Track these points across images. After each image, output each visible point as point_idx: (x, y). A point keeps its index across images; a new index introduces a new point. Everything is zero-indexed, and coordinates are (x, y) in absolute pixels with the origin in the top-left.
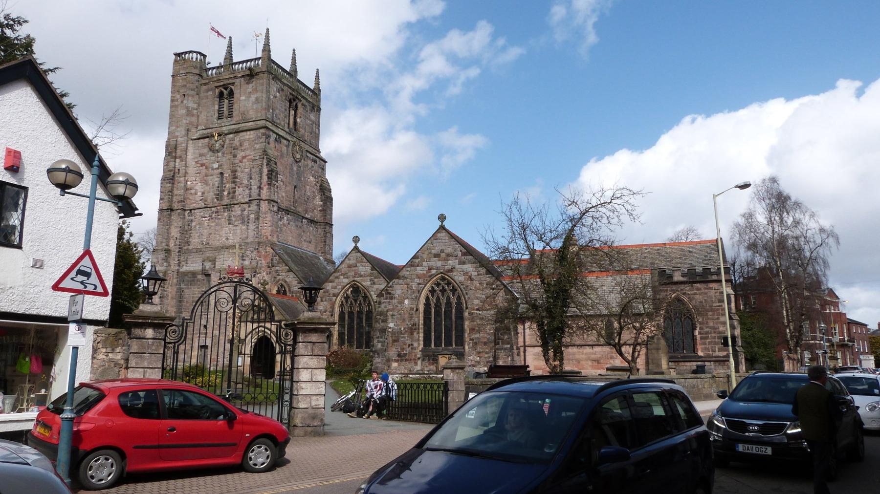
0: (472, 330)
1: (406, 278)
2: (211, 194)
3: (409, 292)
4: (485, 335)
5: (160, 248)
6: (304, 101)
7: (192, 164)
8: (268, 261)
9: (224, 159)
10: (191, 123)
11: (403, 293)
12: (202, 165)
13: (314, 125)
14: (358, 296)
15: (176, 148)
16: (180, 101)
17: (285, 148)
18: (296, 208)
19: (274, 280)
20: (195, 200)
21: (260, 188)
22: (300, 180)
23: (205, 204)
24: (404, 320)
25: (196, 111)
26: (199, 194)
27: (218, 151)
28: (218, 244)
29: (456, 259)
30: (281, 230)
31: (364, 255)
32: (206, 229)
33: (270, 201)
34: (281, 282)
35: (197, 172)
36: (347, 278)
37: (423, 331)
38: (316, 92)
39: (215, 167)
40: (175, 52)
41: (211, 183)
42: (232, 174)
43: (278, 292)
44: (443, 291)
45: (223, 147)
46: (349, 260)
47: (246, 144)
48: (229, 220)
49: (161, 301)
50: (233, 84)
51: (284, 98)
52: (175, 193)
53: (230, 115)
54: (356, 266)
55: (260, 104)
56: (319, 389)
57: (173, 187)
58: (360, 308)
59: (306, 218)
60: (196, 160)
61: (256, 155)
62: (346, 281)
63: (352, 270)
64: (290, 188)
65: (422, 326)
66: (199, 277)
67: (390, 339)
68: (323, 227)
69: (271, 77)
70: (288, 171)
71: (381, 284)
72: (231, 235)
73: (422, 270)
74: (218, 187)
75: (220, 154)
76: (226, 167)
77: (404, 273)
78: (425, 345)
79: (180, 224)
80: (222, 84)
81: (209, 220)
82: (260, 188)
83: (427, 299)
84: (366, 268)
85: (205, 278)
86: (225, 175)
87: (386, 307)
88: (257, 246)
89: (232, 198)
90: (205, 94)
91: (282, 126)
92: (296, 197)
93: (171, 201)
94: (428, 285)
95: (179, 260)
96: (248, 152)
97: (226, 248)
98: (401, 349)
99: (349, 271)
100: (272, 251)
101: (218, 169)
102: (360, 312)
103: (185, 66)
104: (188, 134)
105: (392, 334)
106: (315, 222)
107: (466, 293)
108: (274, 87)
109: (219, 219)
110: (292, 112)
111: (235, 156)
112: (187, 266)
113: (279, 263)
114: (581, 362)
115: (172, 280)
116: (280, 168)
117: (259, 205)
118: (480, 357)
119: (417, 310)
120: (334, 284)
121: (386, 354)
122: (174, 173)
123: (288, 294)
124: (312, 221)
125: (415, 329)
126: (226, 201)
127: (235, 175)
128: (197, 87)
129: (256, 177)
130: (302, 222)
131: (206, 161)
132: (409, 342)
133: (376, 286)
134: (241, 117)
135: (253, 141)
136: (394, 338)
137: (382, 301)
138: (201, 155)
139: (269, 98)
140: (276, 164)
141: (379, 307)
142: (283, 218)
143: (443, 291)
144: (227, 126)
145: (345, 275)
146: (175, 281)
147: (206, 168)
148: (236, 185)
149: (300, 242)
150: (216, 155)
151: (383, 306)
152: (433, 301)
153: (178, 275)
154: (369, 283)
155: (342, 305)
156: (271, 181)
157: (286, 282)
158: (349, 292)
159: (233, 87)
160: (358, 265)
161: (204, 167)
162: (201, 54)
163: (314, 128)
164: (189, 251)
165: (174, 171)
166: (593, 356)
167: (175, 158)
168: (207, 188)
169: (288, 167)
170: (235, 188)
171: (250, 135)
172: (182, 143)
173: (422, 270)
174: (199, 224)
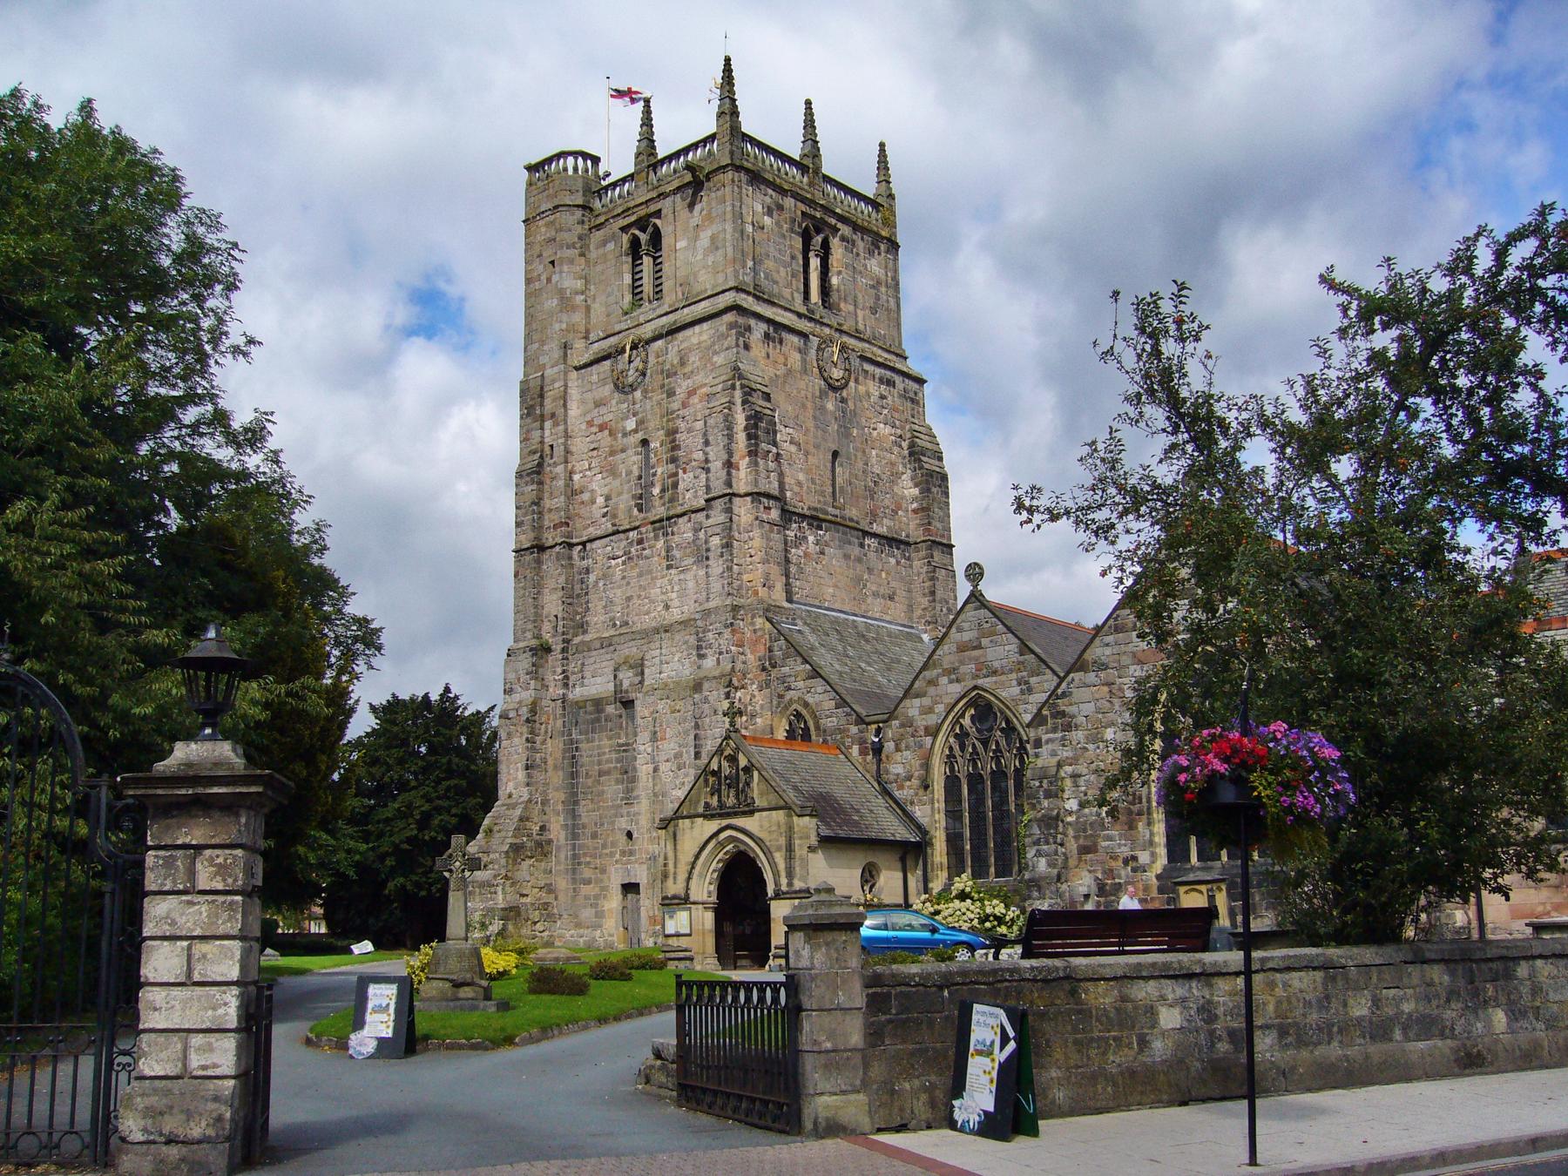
1: (1103, 667)
2: (626, 496)
5: (522, 645)
6: (845, 230)
7: (580, 430)
8: (761, 654)
9: (648, 404)
10: (571, 329)
12: (602, 428)
13: (883, 289)
14: (990, 729)
15: (542, 396)
16: (544, 278)
17: (798, 356)
18: (842, 508)
19: (779, 703)
20: (592, 521)
21: (729, 465)
22: (847, 435)
23: (614, 525)
25: (583, 297)
26: (600, 500)
27: (633, 388)
28: (647, 622)
31: (1001, 614)
32: (619, 587)
33: (756, 496)
34: (794, 706)
35: (592, 446)
36: (958, 681)
38: (883, 203)
39: (629, 429)
40: (526, 163)
41: (622, 469)
42: (668, 440)
43: (791, 735)
45: (644, 374)
46: (960, 630)
47: (694, 359)
48: (668, 558)
49: (529, 776)
50: (658, 214)
52: (547, 506)
53: (658, 293)
54: (979, 647)
55: (720, 252)
56: (214, 1009)
57: (541, 491)
58: (998, 763)
59: (875, 535)
60: (588, 418)
61: (717, 381)
62: (956, 689)
63: (970, 659)
64: (821, 459)
66: (610, 709)
67: (1072, 846)
72: (674, 595)
74: (640, 478)
75: (638, 394)
76: (653, 423)
78: (1171, 857)
79: (562, 579)
80: (633, 218)
81: (624, 563)
82: (729, 465)
84: (1003, 651)
85: (623, 711)
87: (1054, 754)
88: (729, 615)
89: (672, 500)
90: (601, 251)
92: (839, 480)
93: (538, 528)
95: (564, 672)
96: (699, 378)
97: (666, 631)
98: (1104, 872)
99: (962, 663)
100: (768, 625)
101: (636, 431)
102: (999, 775)
104: (565, 355)
105: (1077, 831)
106: (901, 542)
108: (756, 203)
110: (815, 263)
111: (671, 393)
112: (583, 685)
113: (786, 656)
116: (782, 408)
117: (729, 511)
120: (926, 701)
121: (1064, 887)
122: (541, 457)
123: (813, 737)
125: (1140, 813)
126: (659, 511)
127: (674, 441)
128: (580, 238)
129: (718, 439)
130: (862, 545)
131: (611, 416)
132: (1125, 851)
134: (680, 294)
135: (708, 348)
136: (1081, 841)
137: (1044, 738)
139: (742, 232)
140: (767, 397)
142: (805, 538)
144: (650, 320)
146: (559, 723)
147: (610, 435)
148: (677, 467)
150: (630, 397)
151: (1044, 750)
154: (1016, 690)
155: (951, 756)
156: (757, 445)
157: (806, 705)
158: (967, 721)
159: (658, 222)
160: (985, 642)
161: (606, 432)
162: (585, 156)
164: (587, 647)
165: (542, 451)
167: (542, 418)
168: (617, 483)
169: (809, 405)
170: (676, 474)
171: (700, 333)
172: (554, 381)
174: (605, 576)
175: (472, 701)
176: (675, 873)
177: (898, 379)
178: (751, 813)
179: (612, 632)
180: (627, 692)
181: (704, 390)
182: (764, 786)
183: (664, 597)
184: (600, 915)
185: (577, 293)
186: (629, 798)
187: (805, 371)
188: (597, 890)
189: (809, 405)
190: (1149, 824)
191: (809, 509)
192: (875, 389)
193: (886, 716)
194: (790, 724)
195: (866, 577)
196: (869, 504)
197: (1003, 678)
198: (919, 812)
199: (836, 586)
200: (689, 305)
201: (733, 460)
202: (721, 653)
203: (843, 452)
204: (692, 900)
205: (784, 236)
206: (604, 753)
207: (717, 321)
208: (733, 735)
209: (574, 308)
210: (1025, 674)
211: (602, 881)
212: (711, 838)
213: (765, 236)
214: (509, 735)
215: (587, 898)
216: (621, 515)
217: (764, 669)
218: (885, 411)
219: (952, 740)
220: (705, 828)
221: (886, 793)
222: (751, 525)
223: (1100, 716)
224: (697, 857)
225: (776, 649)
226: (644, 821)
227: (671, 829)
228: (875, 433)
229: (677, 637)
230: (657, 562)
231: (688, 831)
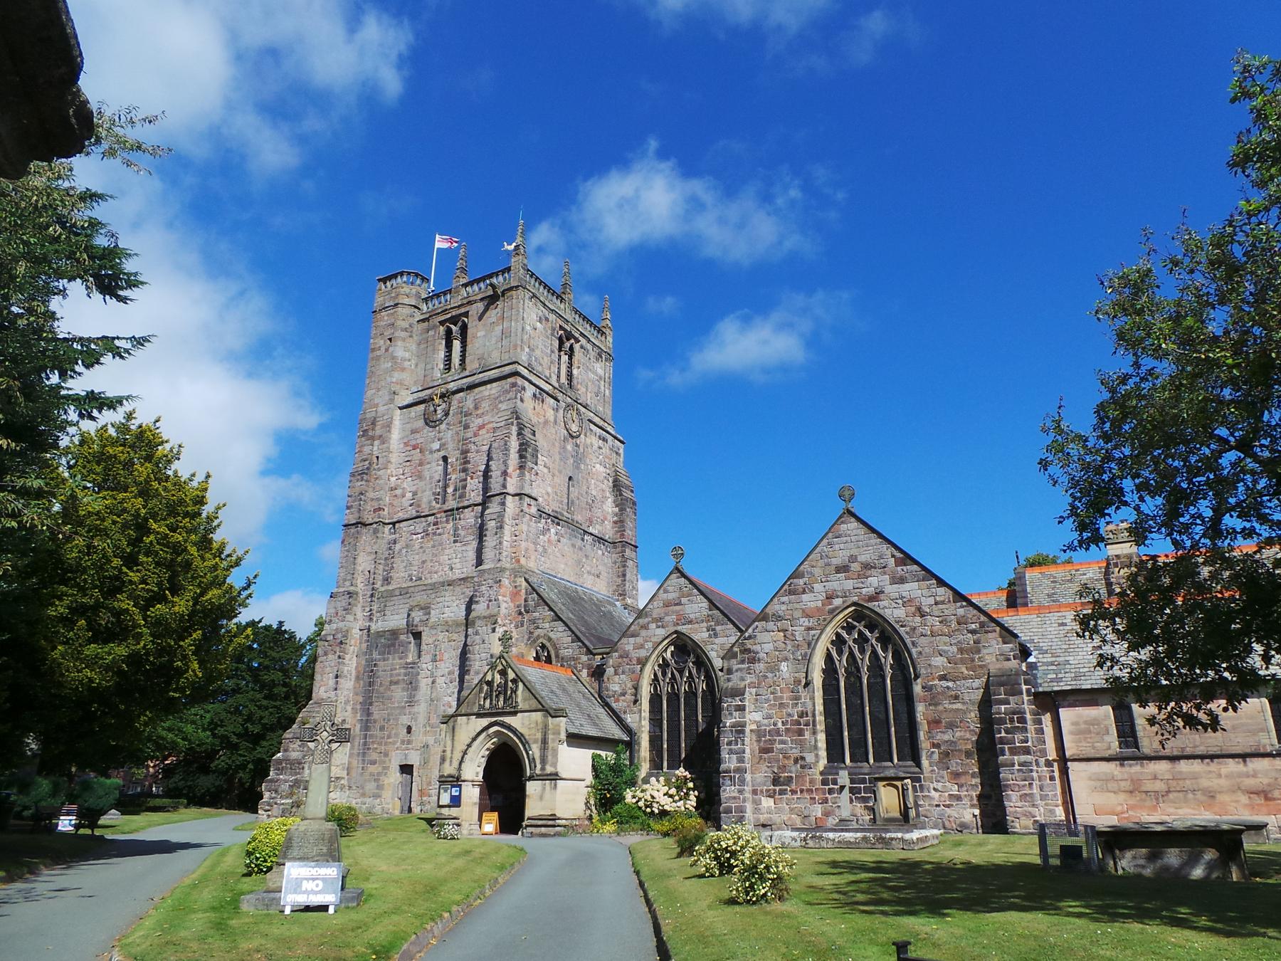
0: (934, 723)
2: (428, 493)
3: (789, 647)
4: (968, 736)
5: (341, 590)
6: (583, 341)
11: (776, 649)
13: (603, 383)
16: (383, 349)
17: (552, 412)
19: (529, 638)
22: (578, 468)
24: (782, 705)
26: (409, 495)
28: (436, 578)
29: (885, 573)
30: (545, 550)
32: (417, 554)
34: (541, 640)
36: (663, 627)
37: (823, 727)
39: (434, 449)
41: (427, 474)
43: (537, 658)
44: (862, 640)
46: (666, 591)
47: (485, 405)
49: (337, 683)
50: (466, 314)
51: (549, 332)
54: (679, 604)
61: (501, 419)
62: (661, 632)
63: (673, 612)
64: (562, 480)
65: (820, 718)
68: (619, 549)
69: (527, 296)
70: (557, 449)
71: (728, 637)
72: (458, 560)
73: (811, 600)
75: (443, 426)
76: (451, 446)
77: (777, 607)
80: (449, 316)
81: (422, 538)
83: (829, 658)
84: (697, 607)
86: (449, 460)
91: (545, 376)
92: (572, 496)
94: (828, 629)
95: (371, 610)
96: (487, 418)
98: (779, 768)
99: (667, 614)
103: (393, 295)
107: (913, 643)
109: (440, 534)
111: (466, 427)
113: (537, 605)
114: (1220, 797)
115: (355, 643)
116: (541, 442)
117: (503, 504)
118: (960, 786)
119: (807, 685)
120: (640, 640)
123: (554, 663)
124: (600, 539)
126: (451, 504)
127: (466, 458)
130: (583, 540)
131: (422, 440)
132: (795, 753)
133: (719, 641)
135: (495, 399)
137: (735, 667)
138: (413, 432)
141: (729, 680)
143: (862, 640)
145: (659, 621)
148: (467, 475)
149: (580, 575)
151: (735, 677)
152: (842, 664)
153: (369, 636)
155: (656, 678)
156: (525, 462)
157: (550, 639)
158: (668, 655)
159: (466, 320)
160: (684, 600)
161: (418, 450)
163: (602, 388)
165: (371, 460)
166: (1250, 783)
167: (373, 438)
170: (466, 480)
171: (491, 389)
173: (811, 600)
175: (302, 629)
176: (451, 758)
177: (610, 438)
178: (514, 713)
179: (410, 584)
180: (417, 626)
181: (491, 425)
182: (527, 694)
183: (449, 562)
184: (380, 787)
185: (405, 360)
186: (411, 702)
187: (555, 422)
188: (380, 769)
189: (557, 444)
190: (814, 733)
191: (553, 511)
192: (597, 443)
193: (608, 650)
194: (537, 653)
195: (584, 560)
196: (588, 514)
197: (696, 626)
198: (629, 719)
199: (566, 564)
200: (484, 372)
201: (508, 471)
202: (490, 601)
203: (575, 478)
204: (462, 778)
205: (548, 338)
206: (396, 669)
207: (503, 382)
208: (505, 655)
209: (403, 370)
210: (713, 623)
211: (384, 762)
212: (482, 731)
213: (537, 335)
214: (326, 654)
215: (372, 774)
216: (423, 506)
217: (520, 613)
218: (601, 457)
219: (656, 668)
220: (478, 724)
221: (606, 705)
222: (518, 515)
223: (777, 653)
224: (469, 746)
225: (530, 599)
226: (422, 719)
227: (451, 724)
228: (594, 469)
229: (458, 589)
230: (447, 538)
231: (464, 726)
